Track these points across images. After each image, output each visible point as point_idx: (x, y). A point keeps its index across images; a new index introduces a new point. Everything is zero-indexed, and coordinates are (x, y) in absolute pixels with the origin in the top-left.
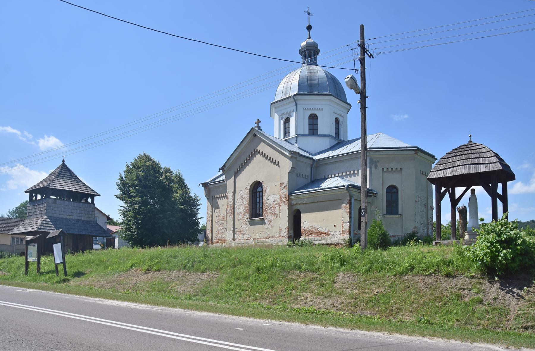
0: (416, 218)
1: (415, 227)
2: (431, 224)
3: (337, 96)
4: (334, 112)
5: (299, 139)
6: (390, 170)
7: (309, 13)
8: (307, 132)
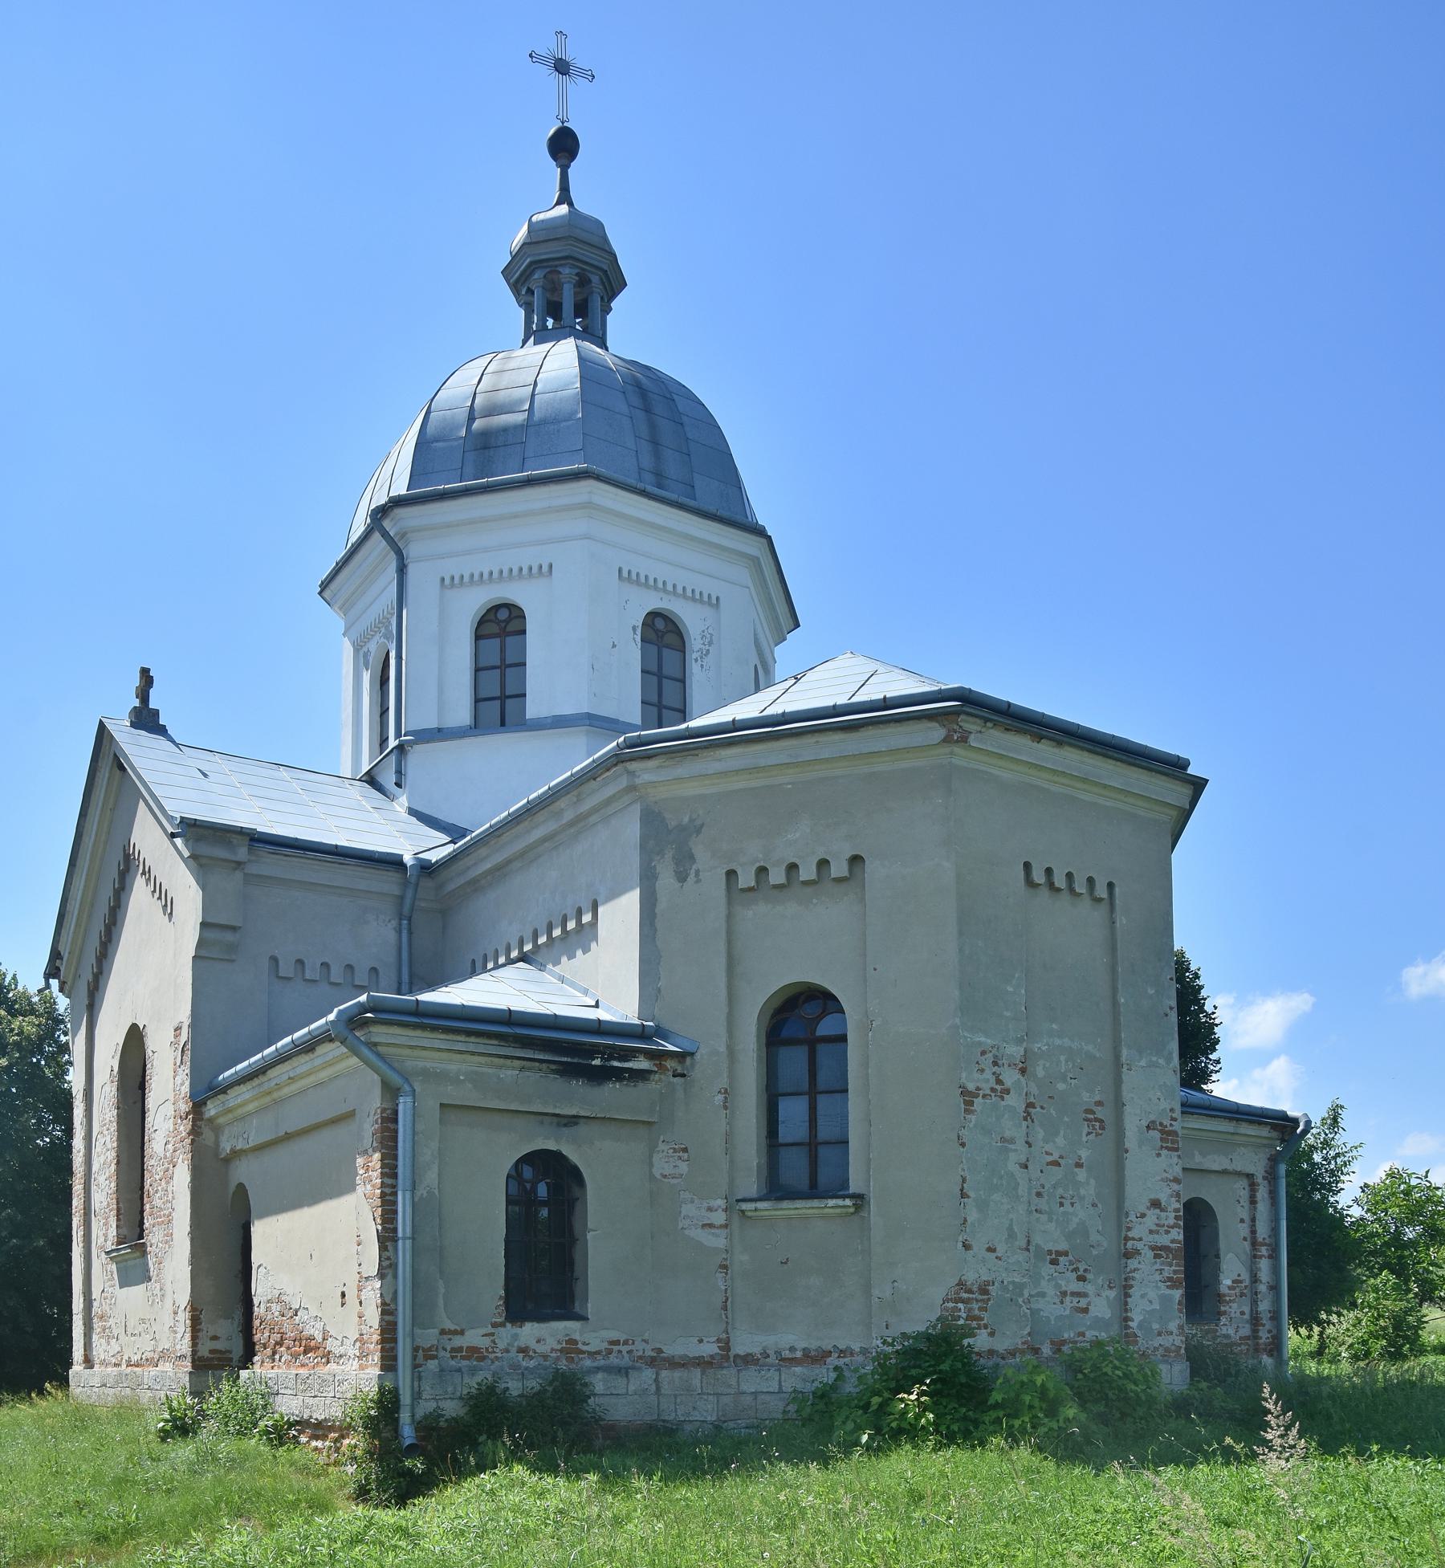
0: (973, 1216)
1: (961, 1284)
2: (1153, 1248)
3: (660, 486)
4: (626, 577)
5: (418, 756)
6: (813, 876)
7: (562, 67)
8: (462, 715)
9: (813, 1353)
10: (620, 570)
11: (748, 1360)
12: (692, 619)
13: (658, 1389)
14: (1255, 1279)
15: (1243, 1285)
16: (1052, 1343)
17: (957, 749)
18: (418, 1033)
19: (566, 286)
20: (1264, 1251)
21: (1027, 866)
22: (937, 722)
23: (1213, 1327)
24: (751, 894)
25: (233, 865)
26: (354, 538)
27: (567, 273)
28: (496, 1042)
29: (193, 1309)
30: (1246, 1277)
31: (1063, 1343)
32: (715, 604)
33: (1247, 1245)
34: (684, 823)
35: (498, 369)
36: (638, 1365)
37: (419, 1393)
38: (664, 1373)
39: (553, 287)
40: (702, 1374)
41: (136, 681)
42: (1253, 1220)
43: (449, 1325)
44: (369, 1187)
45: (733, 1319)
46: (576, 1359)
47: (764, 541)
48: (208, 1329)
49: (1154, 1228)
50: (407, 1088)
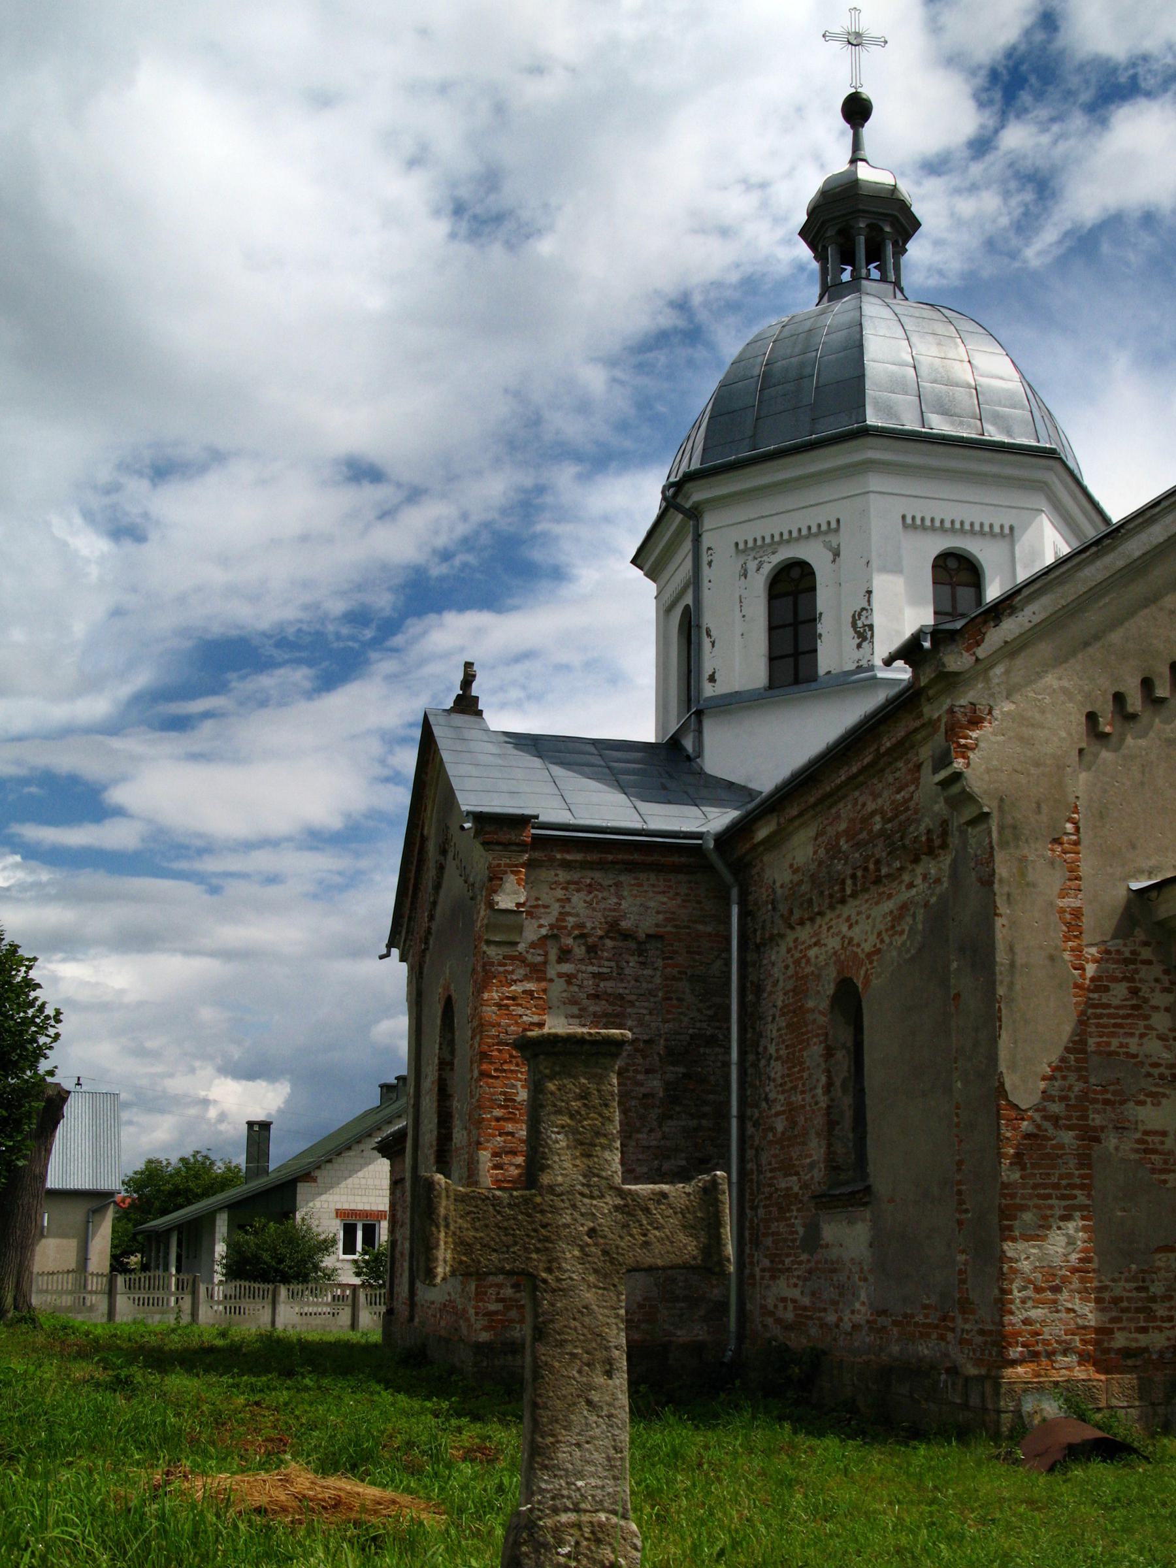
10: (904, 517)
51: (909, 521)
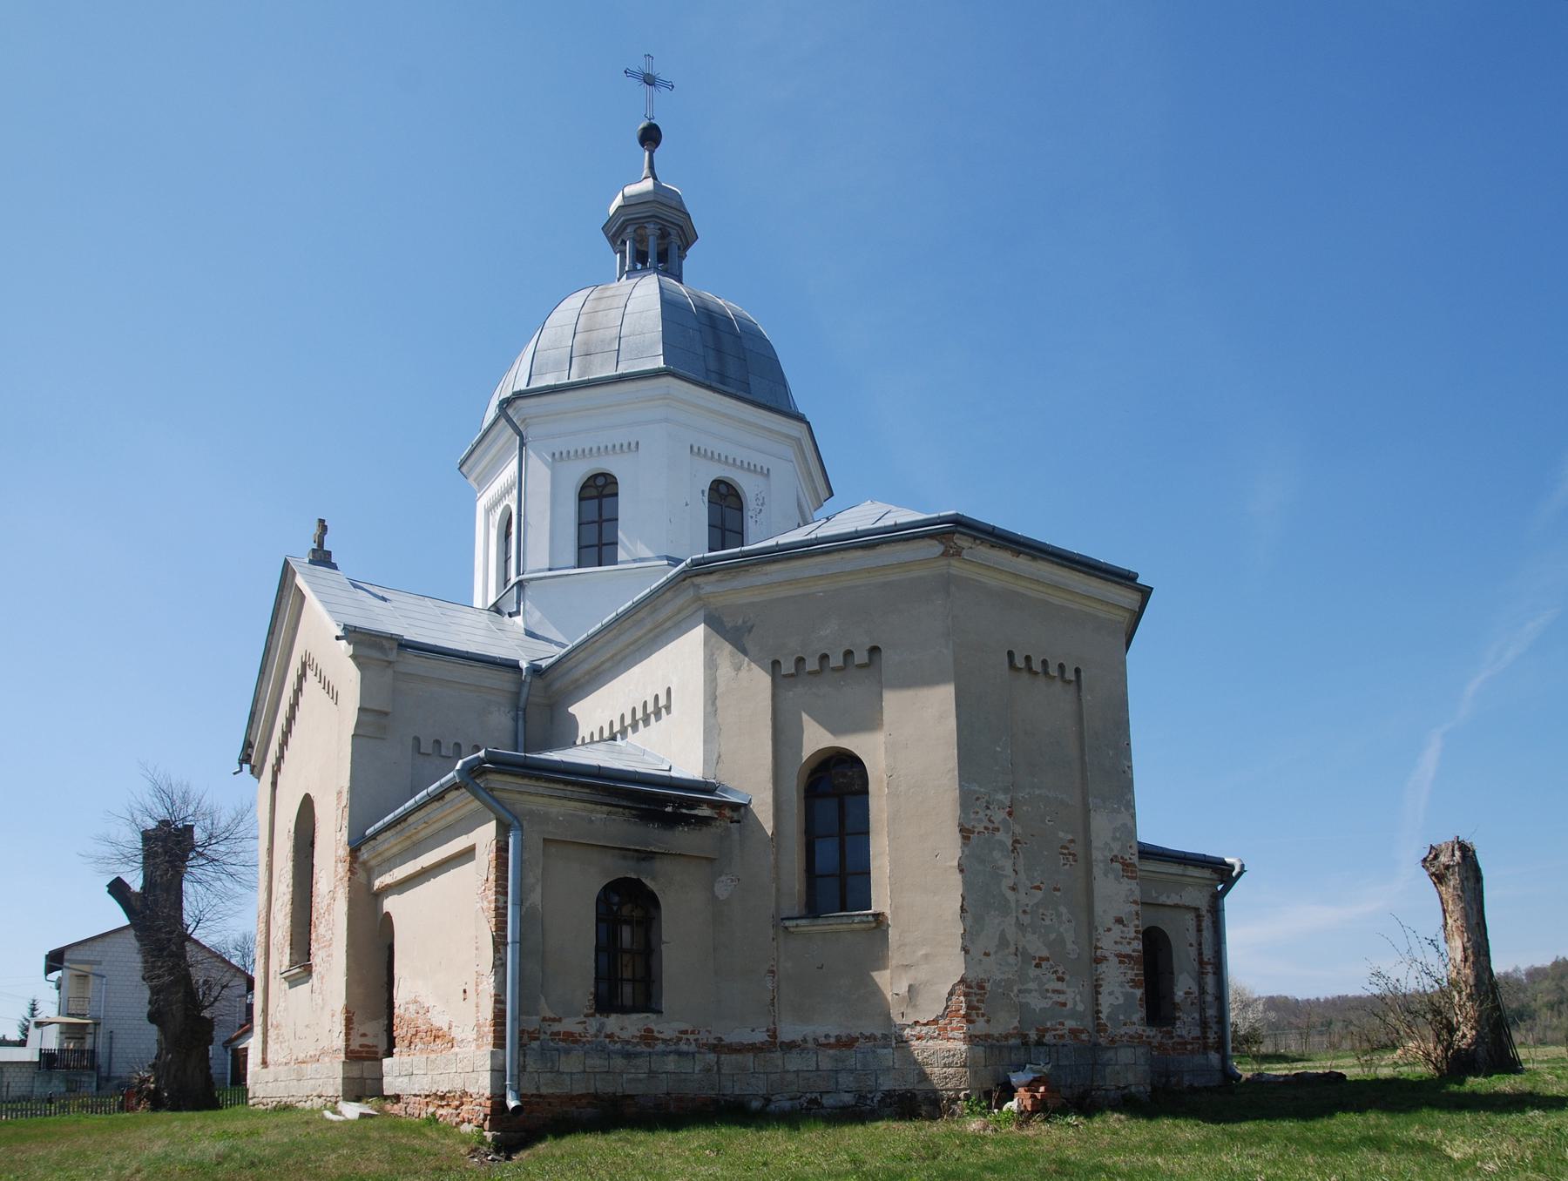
2: (1118, 956)
7: (649, 80)
9: (844, 1039)
10: (692, 447)
11: (790, 1046)
12: (748, 486)
13: (719, 1069)
14: (1202, 991)
15: (1193, 996)
16: (1037, 1029)
17: (954, 562)
18: (526, 781)
19: (651, 238)
20: (1209, 968)
21: (1010, 654)
22: (937, 540)
23: (1169, 1028)
24: (792, 679)
25: (386, 664)
26: (486, 425)
27: (652, 230)
28: (588, 791)
29: (347, 1012)
30: (1195, 989)
31: (1047, 1030)
32: (767, 474)
33: (1196, 964)
34: (738, 624)
35: (597, 297)
36: (702, 1050)
37: (524, 1067)
38: (723, 1057)
39: (639, 240)
40: (755, 1057)
41: (314, 529)
42: (1200, 944)
43: (550, 1014)
44: (485, 903)
45: (779, 1013)
46: (652, 1044)
47: (804, 426)
48: (358, 1028)
49: (1118, 939)
50: (516, 824)
51: (696, 449)
